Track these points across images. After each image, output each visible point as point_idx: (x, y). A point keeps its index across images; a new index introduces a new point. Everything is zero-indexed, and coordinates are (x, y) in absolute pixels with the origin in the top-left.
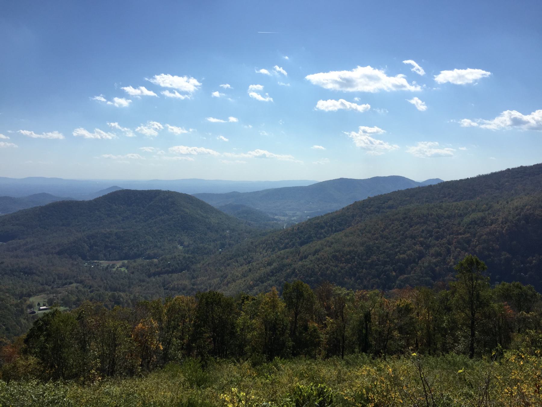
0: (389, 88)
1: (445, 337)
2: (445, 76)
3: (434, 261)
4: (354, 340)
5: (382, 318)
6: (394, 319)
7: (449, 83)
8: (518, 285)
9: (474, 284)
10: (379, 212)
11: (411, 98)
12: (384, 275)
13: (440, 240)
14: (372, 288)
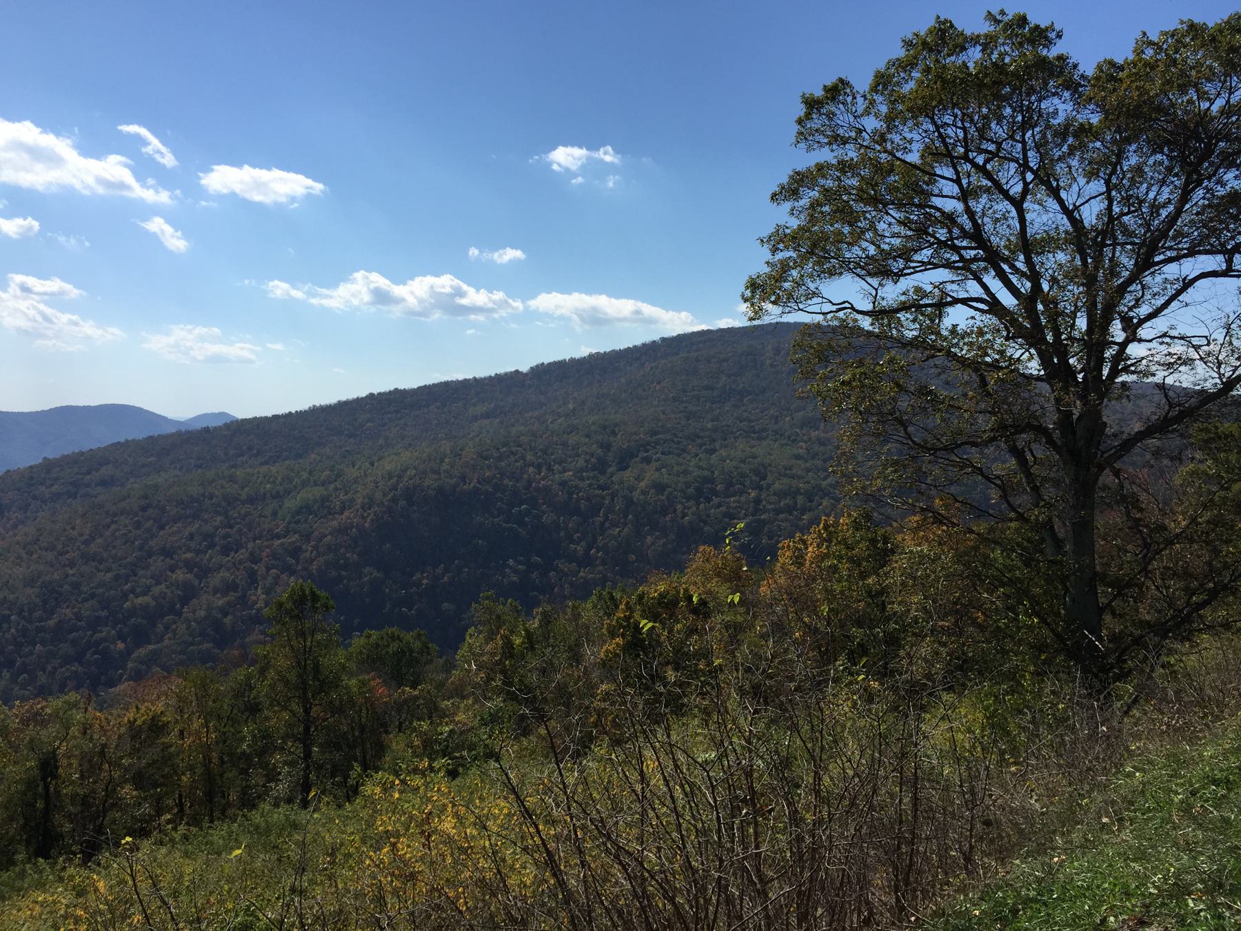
0: (88, 187)
1: (247, 774)
2: (224, 178)
3: (220, 602)
4: (12, 832)
5: (90, 761)
6: (121, 758)
7: (233, 195)
8: (393, 633)
9: (308, 644)
10: (74, 496)
11: (146, 219)
12: (95, 653)
13: (232, 554)
14: (62, 689)
